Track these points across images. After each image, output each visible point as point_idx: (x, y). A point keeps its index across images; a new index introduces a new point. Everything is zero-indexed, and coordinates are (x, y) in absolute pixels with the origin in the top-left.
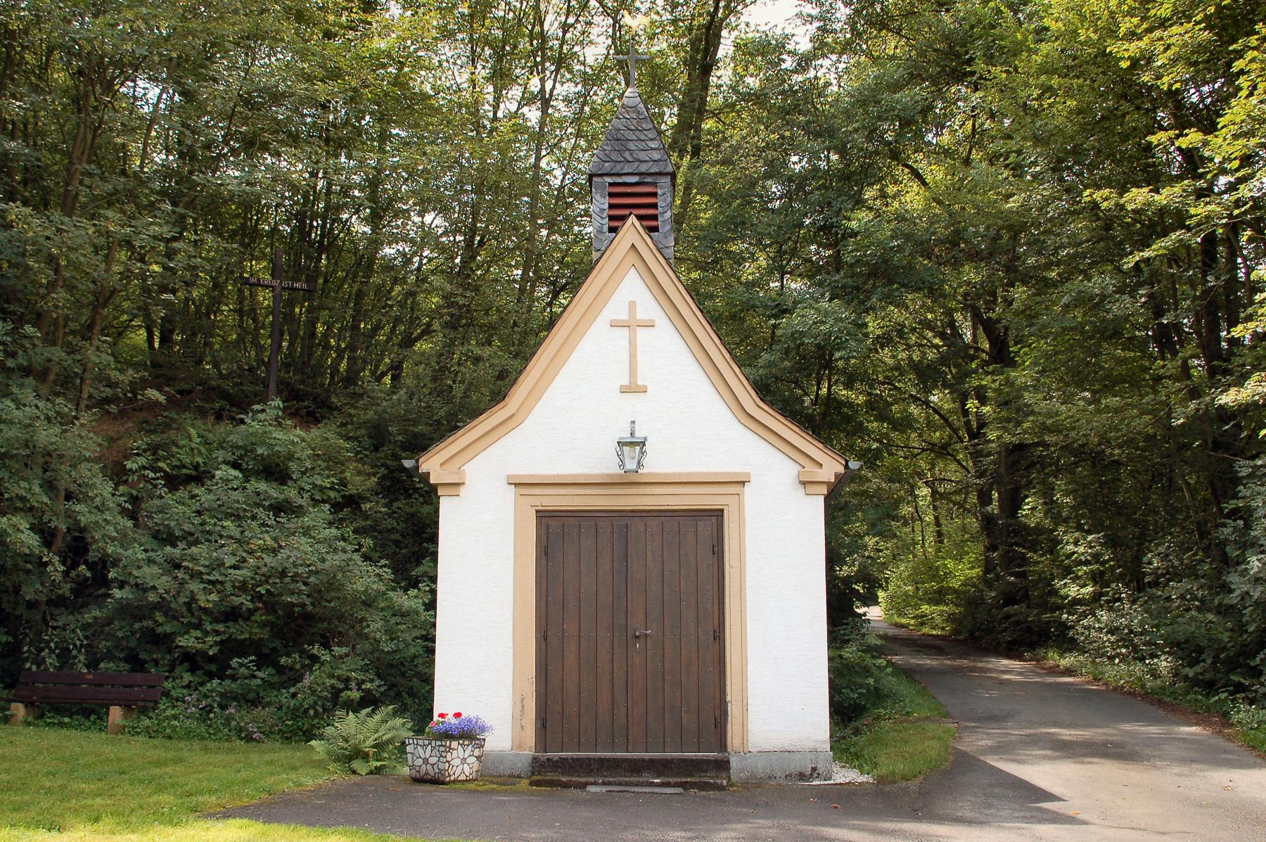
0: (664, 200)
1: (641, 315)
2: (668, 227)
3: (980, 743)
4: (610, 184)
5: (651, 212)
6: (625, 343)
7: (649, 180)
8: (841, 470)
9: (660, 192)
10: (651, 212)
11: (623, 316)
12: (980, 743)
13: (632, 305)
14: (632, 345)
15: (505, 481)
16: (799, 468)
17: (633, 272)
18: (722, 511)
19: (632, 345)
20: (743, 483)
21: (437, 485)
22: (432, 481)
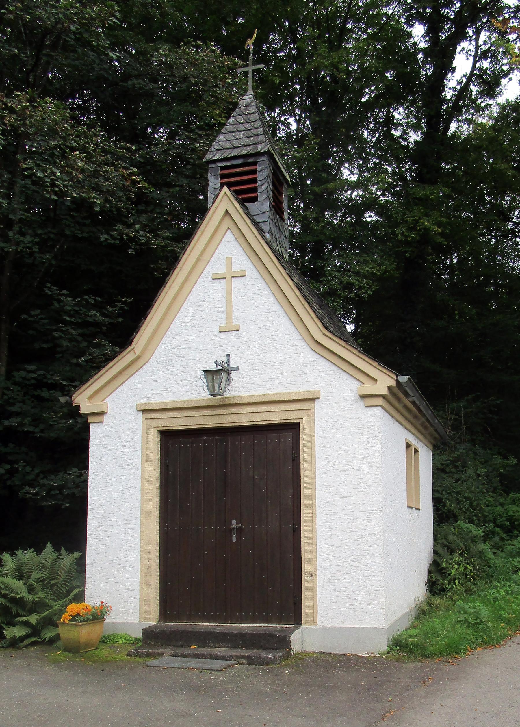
0: (262, 175)
1: (236, 268)
2: (264, 196)
3: (20, 94)
4: (223, 168)
5: (224, 172)
6: (223, 292)
7: (251, 160)
8: (393, 383)
9: (259, 169)
10: (224, 172)
11: (221, 270)
12: (20, 94)
13: (229, 259)
14: (229, 293)
15: (136, 411)
16: (359, 384)
17: (229, 234)
18: (298, 424)
19: (229, 293)
20: (313, 400)
21: (87, 415)
22: (82, 411)
